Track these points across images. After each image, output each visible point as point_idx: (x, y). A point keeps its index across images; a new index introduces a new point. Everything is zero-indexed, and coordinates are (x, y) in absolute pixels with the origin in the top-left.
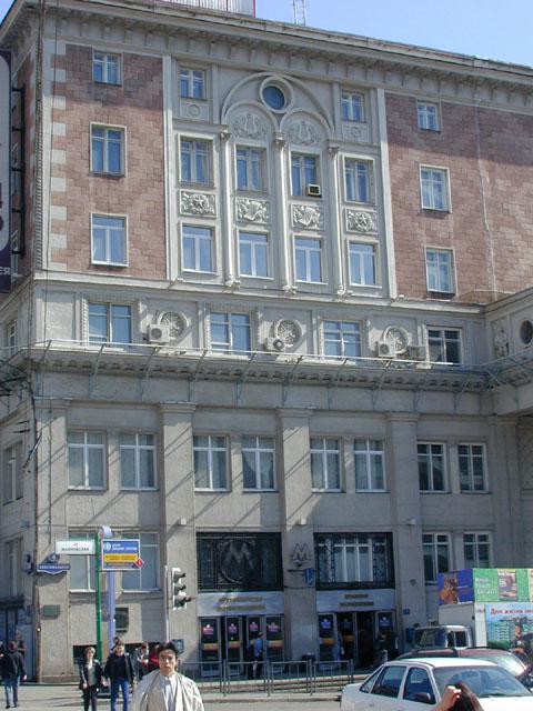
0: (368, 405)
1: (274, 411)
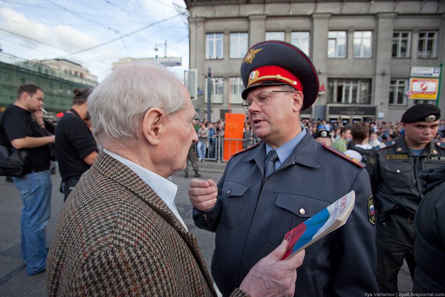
0: (417, 11)
1: (310, 17)
